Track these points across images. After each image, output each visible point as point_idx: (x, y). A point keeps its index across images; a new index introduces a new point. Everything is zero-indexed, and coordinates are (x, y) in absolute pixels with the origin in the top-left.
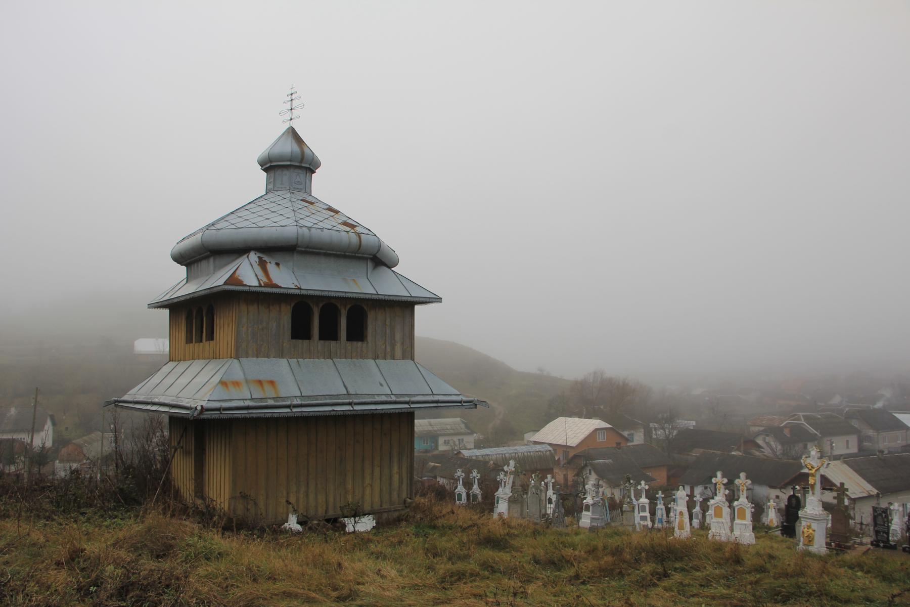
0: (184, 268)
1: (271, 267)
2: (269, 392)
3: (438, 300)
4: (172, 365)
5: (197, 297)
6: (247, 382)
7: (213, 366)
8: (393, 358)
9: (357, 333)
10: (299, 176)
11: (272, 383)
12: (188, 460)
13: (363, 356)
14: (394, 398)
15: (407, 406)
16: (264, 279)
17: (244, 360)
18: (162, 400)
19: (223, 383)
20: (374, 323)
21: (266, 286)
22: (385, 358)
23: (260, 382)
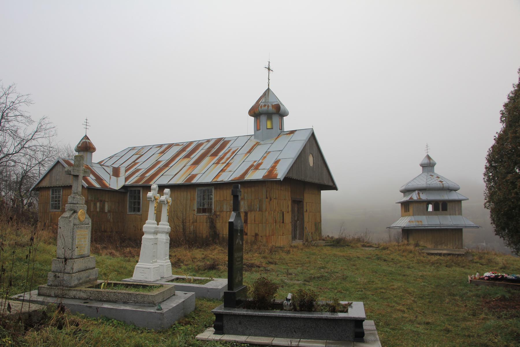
0: (403, 194)
1: (421, 194)
2: (420, 223)
3: (467, 199)
4: (402, 217)
5: (235, 308)
6: (415, 221)
7: (409, 217)
8: (455, 215)
9: (445, 208)
10: (430, 168)
11: (421, 221)
12: (288, 193)
13: (446, 215)
14: (453, 225)
15: (440, 227)
16: (418, 197)
17: (415, 216)
18: (398, 226)
19: (409, 221)
20: (449, 206)
21: (419, 199)
22: (453, 215)
23: (418, 221)
